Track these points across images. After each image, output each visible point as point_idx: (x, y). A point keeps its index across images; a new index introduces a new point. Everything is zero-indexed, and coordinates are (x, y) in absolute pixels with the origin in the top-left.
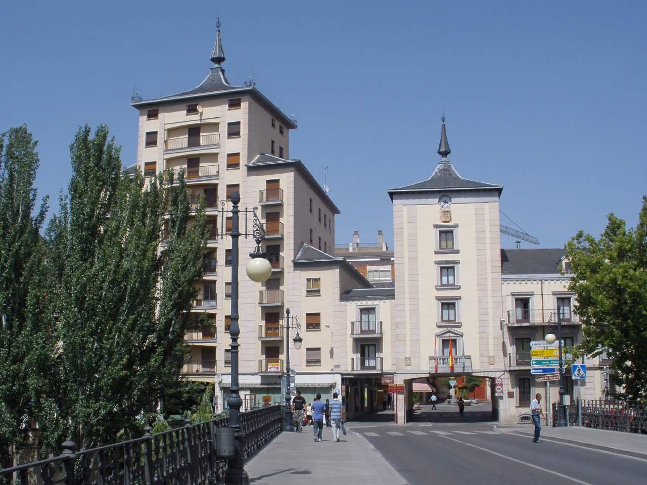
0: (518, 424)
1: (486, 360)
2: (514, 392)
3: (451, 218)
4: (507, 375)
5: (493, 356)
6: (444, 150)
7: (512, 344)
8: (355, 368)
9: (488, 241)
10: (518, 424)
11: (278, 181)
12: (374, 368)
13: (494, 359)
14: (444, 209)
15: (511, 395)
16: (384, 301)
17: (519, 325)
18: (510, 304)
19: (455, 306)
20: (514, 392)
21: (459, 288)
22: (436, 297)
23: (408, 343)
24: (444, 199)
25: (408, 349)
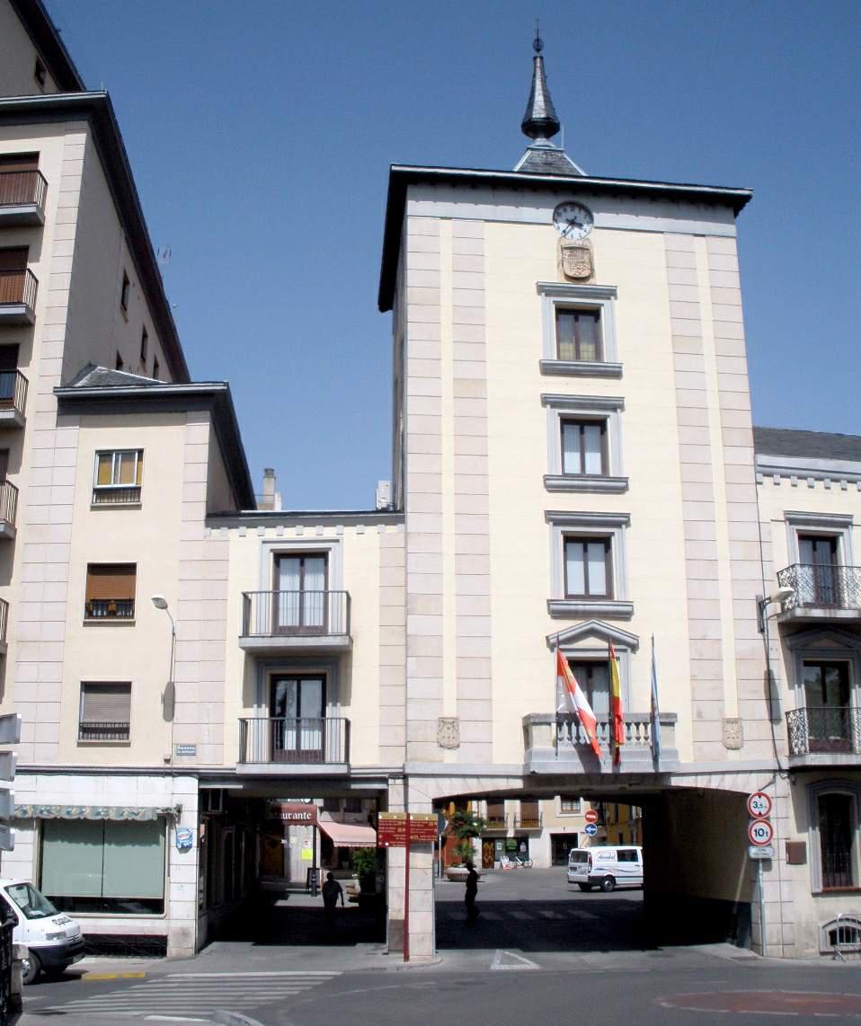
0: (823, 954)
1: (716, 732)
2: (804, 844)
4: (783, 785)
5: (735, 721)
6: (543, 116)
7: (795, 680)
8: (250, 756)
9: (709, 347)
10: (823, 954)
11: (33, 157)
12: (318, 756)
13: (741, 730)
14: (567, 242)
15: (796, 854)
16: (360, 528)
17: (828, 615)
18: (784, 549)
19: (608, 547)
20: (804, 844)
21: (620, 487)
22: (548, 513)
23: (449, 670)
24: (570, 214)
25: (449, 688)
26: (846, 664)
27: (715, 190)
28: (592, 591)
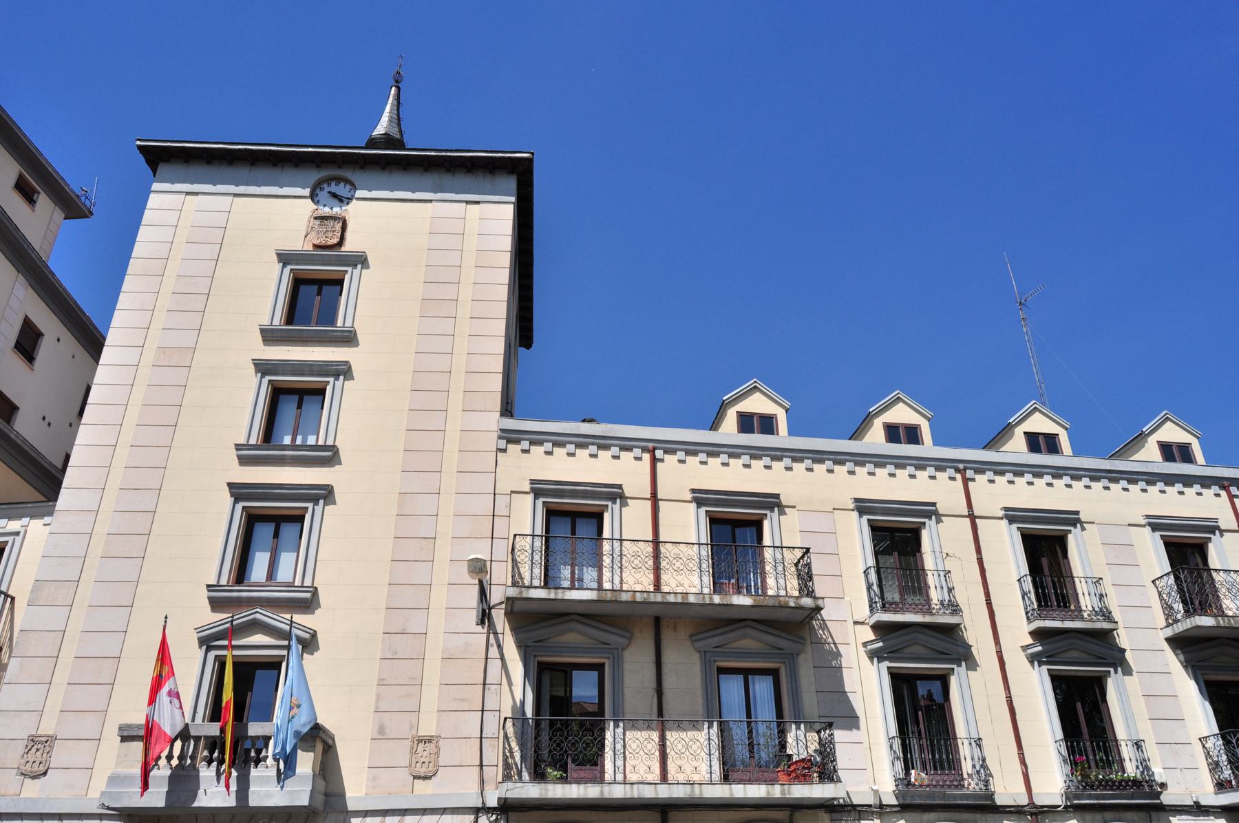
1: (400, 752)
3: (342, 238)
5: (428, 740)
26: (539, 663)
27: (490, 155)
28: (615, 588)
